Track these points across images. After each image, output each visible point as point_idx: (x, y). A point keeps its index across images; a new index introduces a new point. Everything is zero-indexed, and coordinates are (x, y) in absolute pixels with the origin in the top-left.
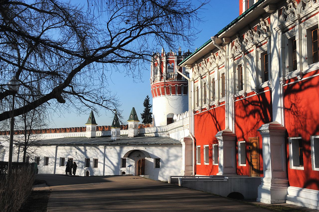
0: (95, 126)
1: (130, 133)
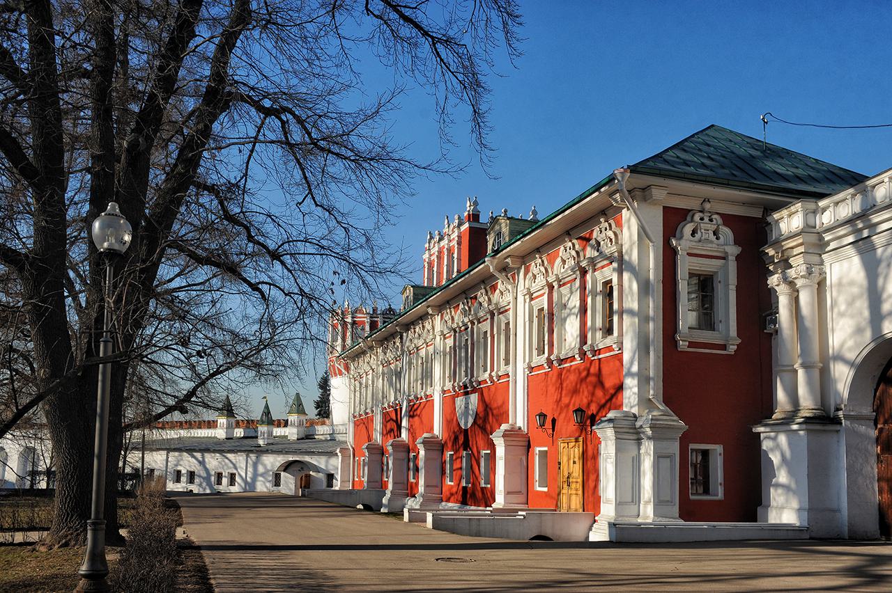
0: (233, 420)
1: (291, 433)
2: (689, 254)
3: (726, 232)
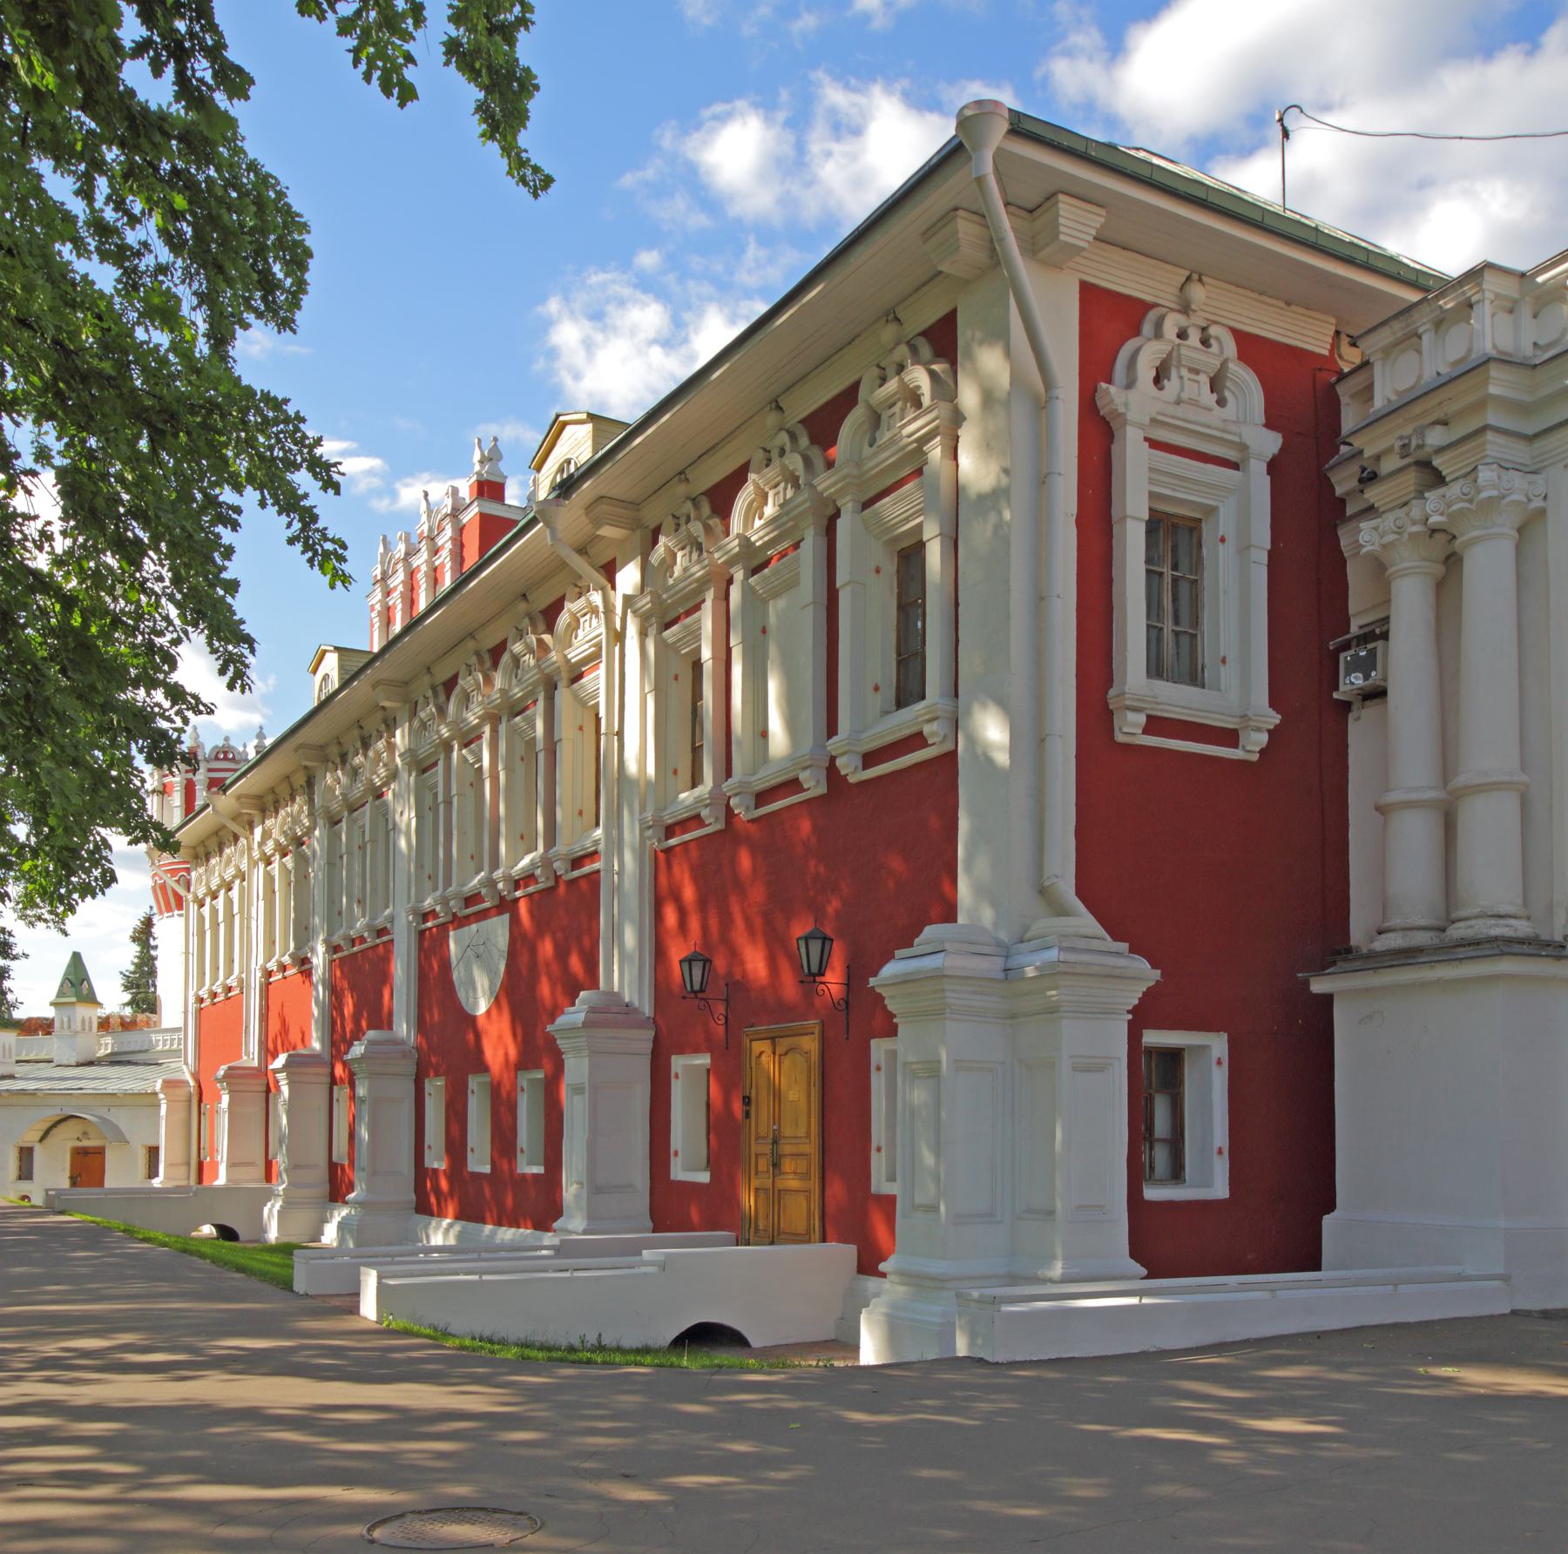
2: (1155, 444)
3: (1246, 382)
